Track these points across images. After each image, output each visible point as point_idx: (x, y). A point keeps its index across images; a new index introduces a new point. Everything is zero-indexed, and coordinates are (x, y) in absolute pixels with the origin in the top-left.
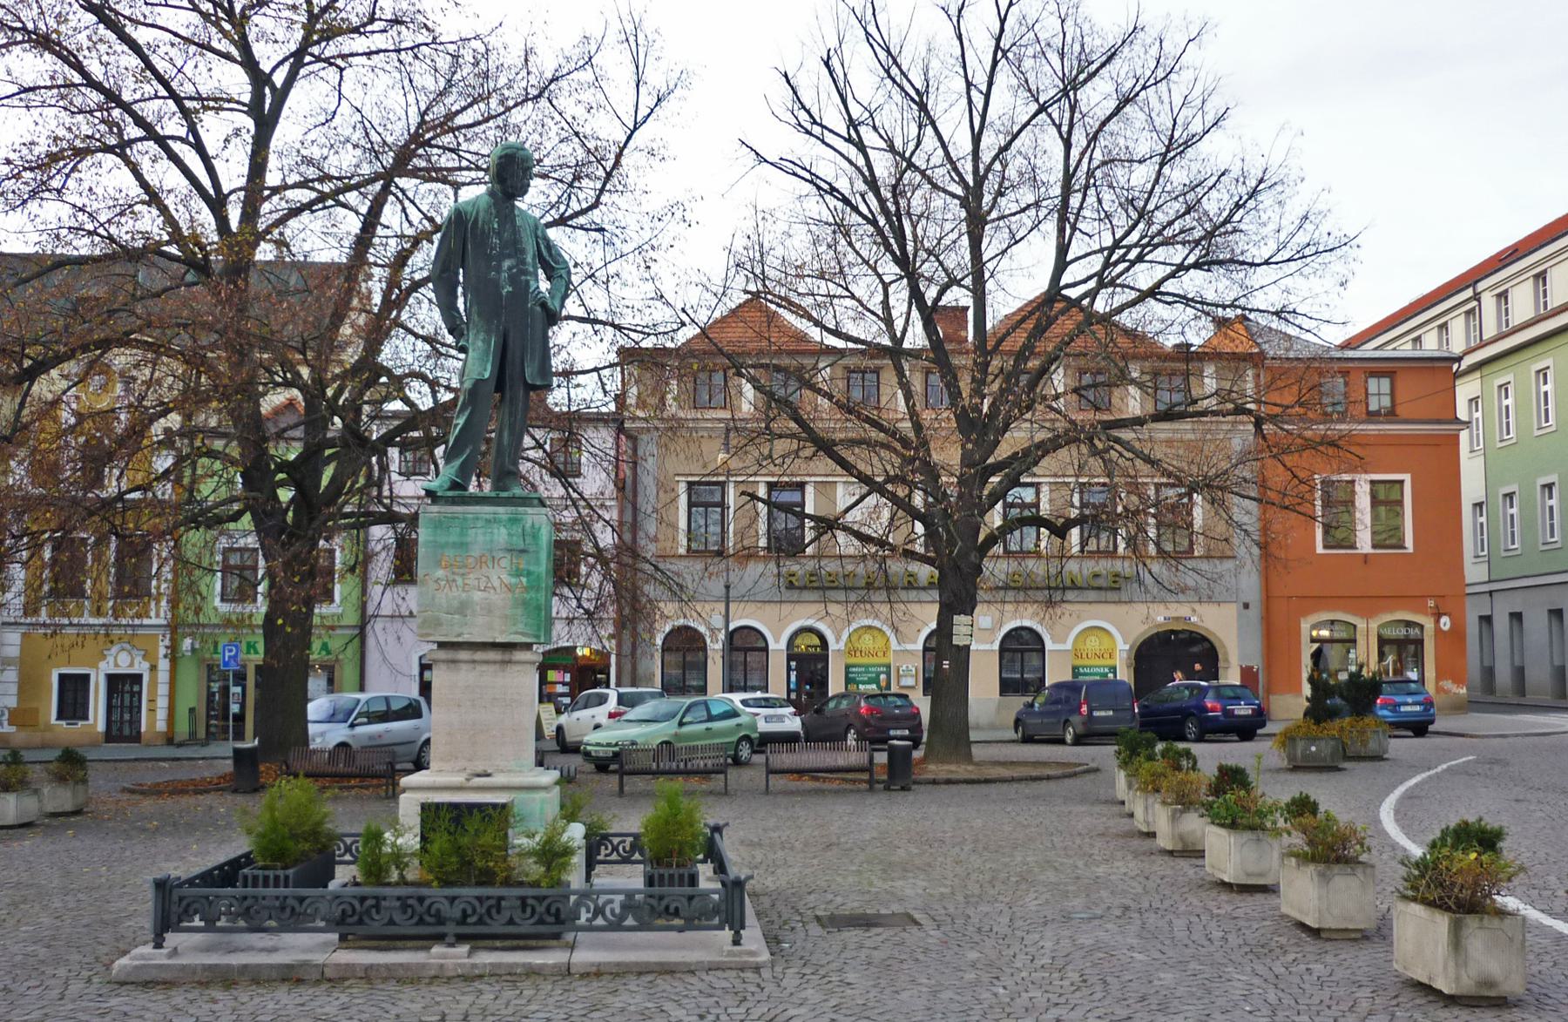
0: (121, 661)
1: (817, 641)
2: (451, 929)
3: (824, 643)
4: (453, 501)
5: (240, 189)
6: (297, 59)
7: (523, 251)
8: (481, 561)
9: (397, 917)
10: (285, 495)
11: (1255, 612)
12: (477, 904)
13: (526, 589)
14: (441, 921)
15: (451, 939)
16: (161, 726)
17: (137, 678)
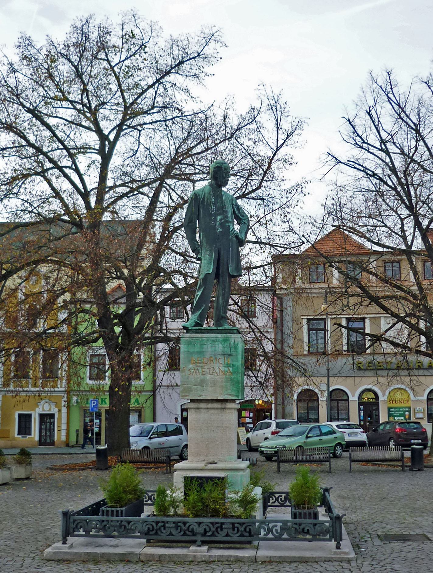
0: (45, 408)
1: (373, 396)
2: (199, 538)
4: (197, 332)
6: (120, 128)
7: (226, 212)
8: (210, 360)
9: (174, 532)
12: (211, 525)
13: (232, 373)
14: (194, 534)
15: (199, 543)
16: (63, 438)
17: (52, 416)
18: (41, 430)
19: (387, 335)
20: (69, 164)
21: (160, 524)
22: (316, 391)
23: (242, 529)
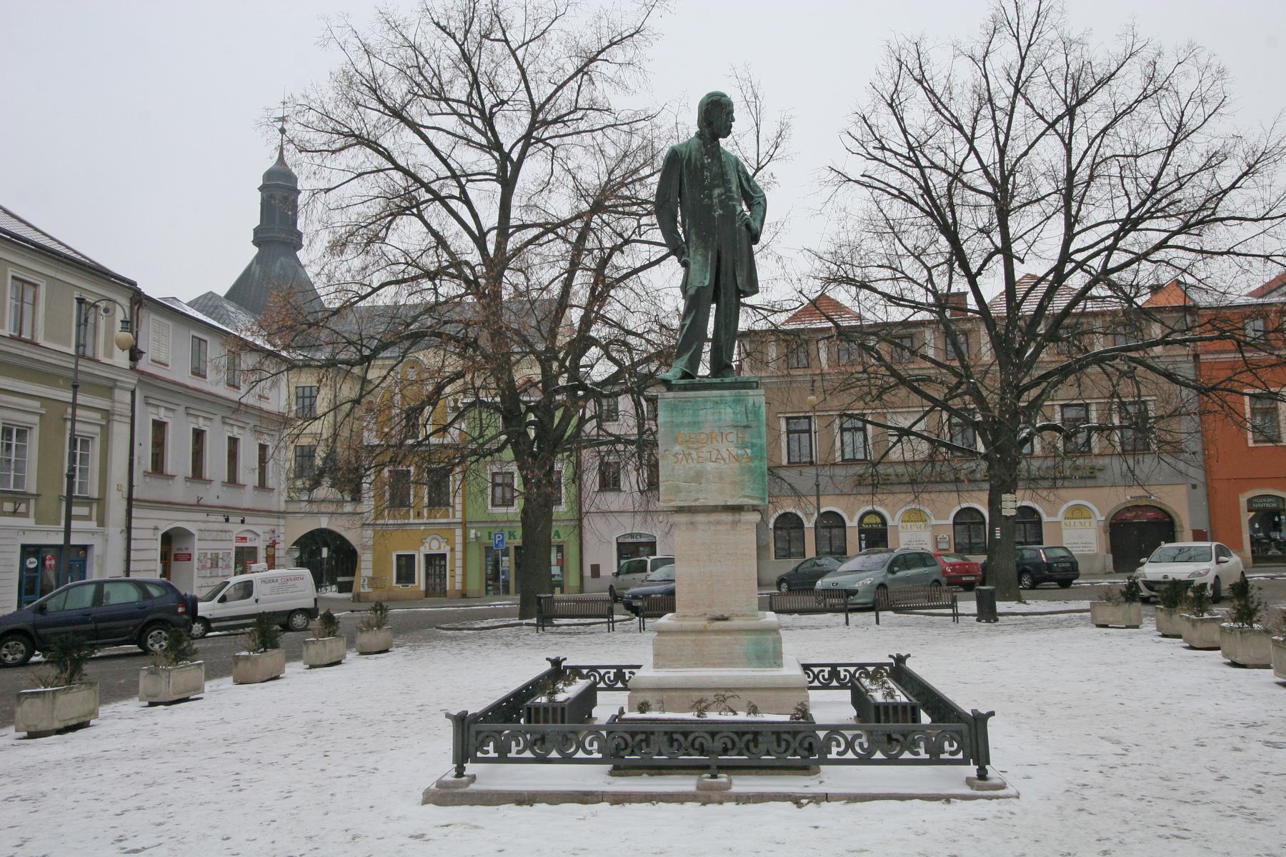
0: (435, 547)
1: (879, 520)
3: (884, 522)
4: (685, 388)
5: (494, 228)
6: (527, 140)
7: (729, 181)
8: (711, 437)
10: (532, 433)
11: (1201, 491)
12: (736, 738)
13: (751, 459)
16: (458, 586)
17: (443, 556)
18: (428, 575)
19: (914, 429)
20: (456, 192)
21: (639, 737)
22: (800, 514)
23: (795, 744)
